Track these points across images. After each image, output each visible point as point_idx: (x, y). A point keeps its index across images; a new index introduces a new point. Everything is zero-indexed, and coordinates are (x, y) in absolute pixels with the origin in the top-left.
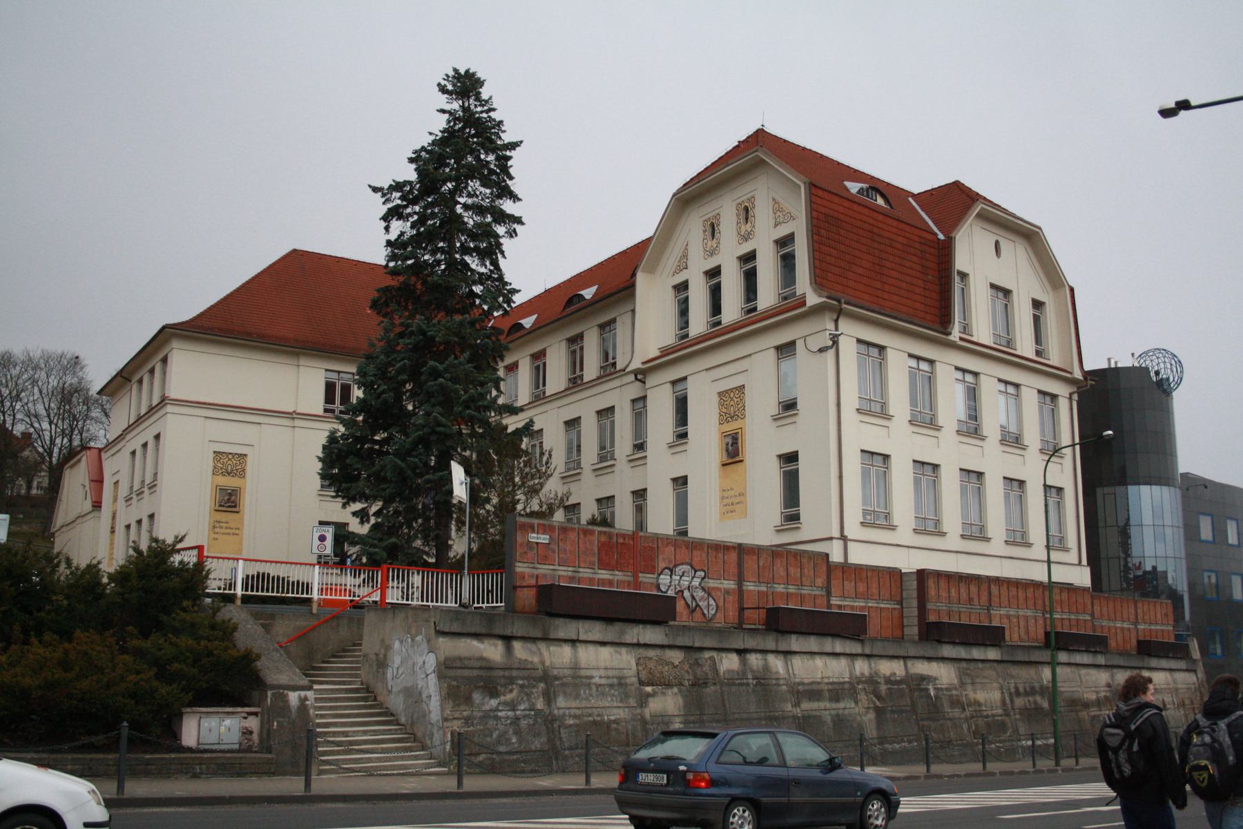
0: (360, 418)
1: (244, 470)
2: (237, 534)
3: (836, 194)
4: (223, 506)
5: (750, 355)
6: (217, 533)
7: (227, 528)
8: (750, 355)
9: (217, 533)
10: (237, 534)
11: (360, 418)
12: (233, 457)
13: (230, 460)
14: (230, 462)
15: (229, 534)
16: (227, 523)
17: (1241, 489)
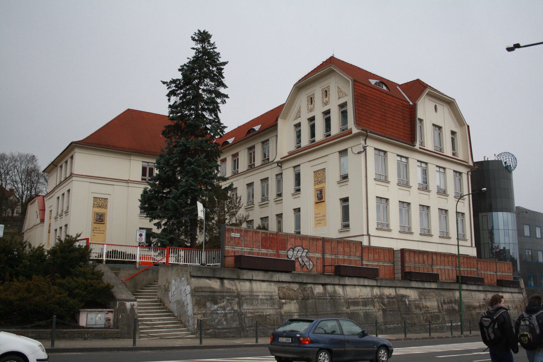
0: (157, 183)
1: (106, 205)
2: (104, 233)
3: (365, 85)
4: (97, 221)
5: (328, 155)
6: (95, 233)
7: (99, 230)
8: (328, 155)
9: (95, 233)
10: (104, 233)
11: (157, 183)
12: (102, 200)
13: (100, 201)
14: (100, 202)
15: (100, 233)
16: (99, 228)
17: (542, 213)
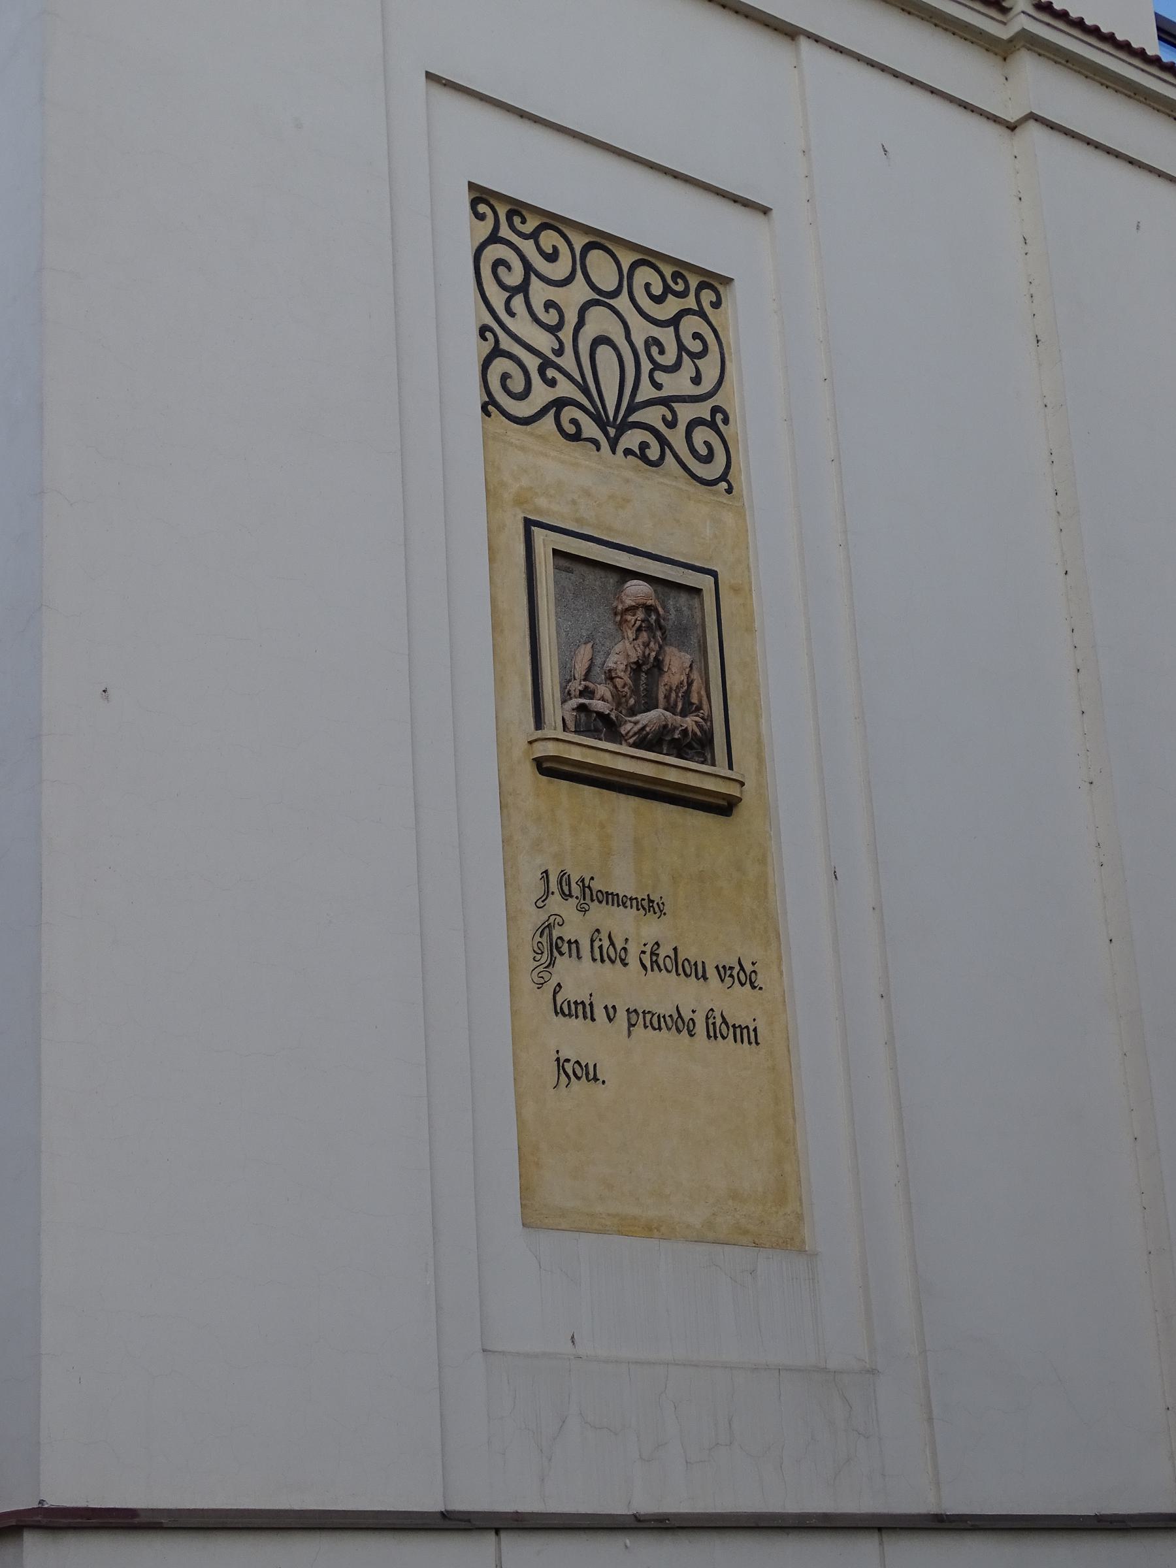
0: (692, 922)
1: (717, 419)
2: (745, 1034)
3: (444, 476)
4: (606, 727)
5: (789, 32)
6: (583, 1010)
7: (653, 961)
8: (789, 32)
9: (583, 1010)
10: (745, 1034)
11: (692, 922)
12: (626, 278)
13: (602, 298)
14: (599, 322)
15: (680, 1023)
16: (650, 906)
17: (1174, 22)
